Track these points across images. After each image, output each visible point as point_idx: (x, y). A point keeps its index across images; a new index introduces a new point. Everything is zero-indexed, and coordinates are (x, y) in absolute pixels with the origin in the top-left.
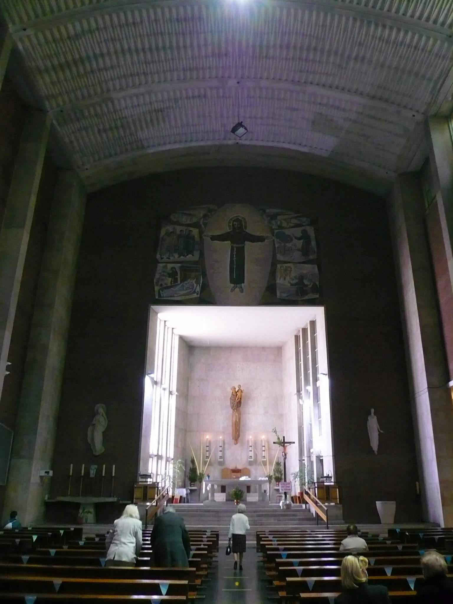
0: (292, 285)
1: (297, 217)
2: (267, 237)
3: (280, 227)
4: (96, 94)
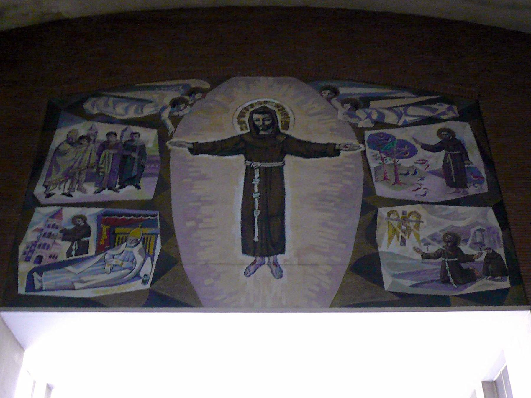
3: (379, 124)
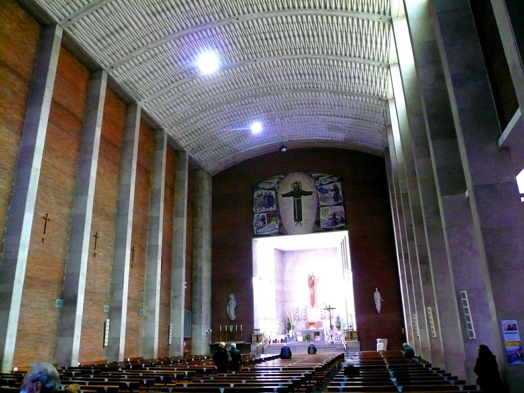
1: (331, 177)
3: (321, 185)
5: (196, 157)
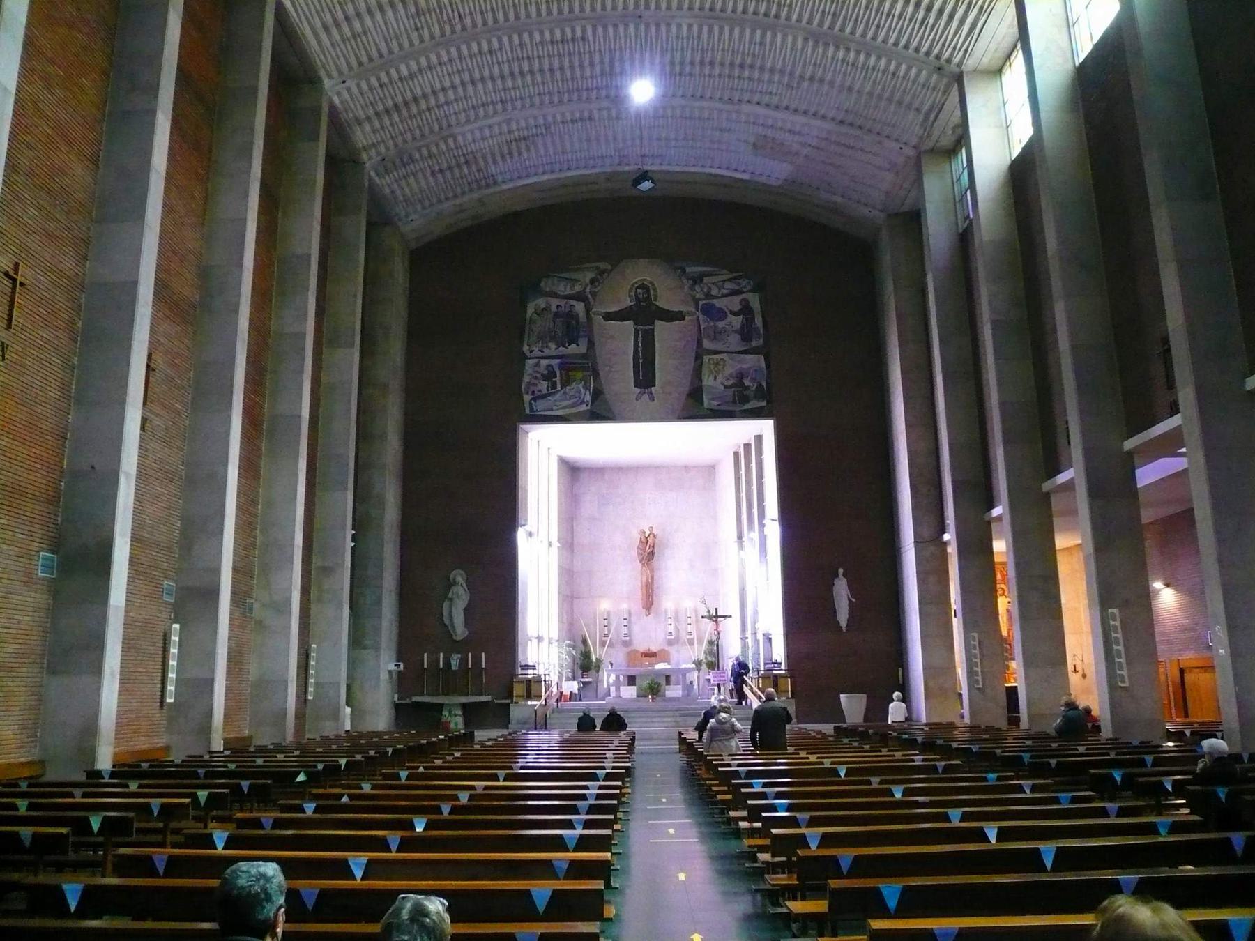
0: (726, 387)
1: (735, 278)
2: (689, 314)
3: (708, 296)
4: (432, 131)
5: (385, 183)
